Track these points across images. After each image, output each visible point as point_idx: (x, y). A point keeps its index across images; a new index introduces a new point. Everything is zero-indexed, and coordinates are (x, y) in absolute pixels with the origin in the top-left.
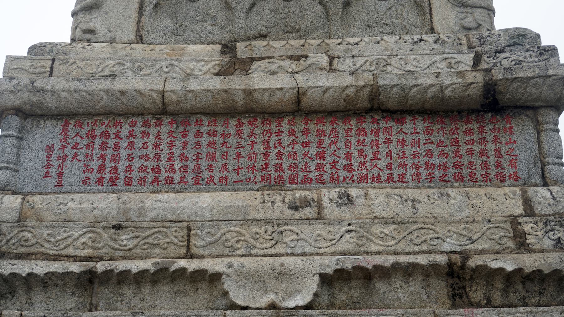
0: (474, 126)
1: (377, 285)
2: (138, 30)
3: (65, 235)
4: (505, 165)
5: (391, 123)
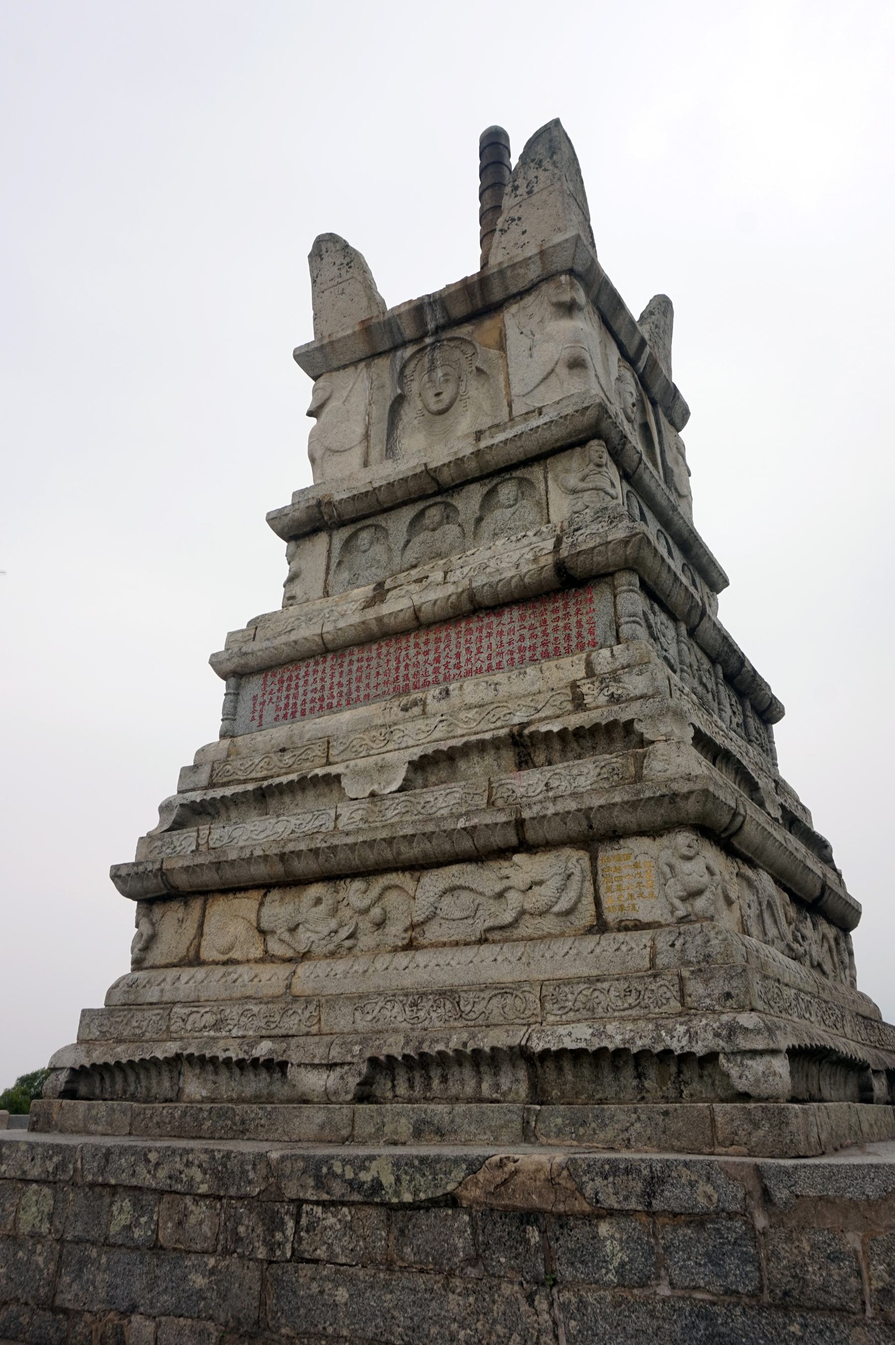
0: (560, 604)
1: (459, 764)
2: (325, 587)
3: (250, 763)
4: (585, 634)
5: (493, 618)
